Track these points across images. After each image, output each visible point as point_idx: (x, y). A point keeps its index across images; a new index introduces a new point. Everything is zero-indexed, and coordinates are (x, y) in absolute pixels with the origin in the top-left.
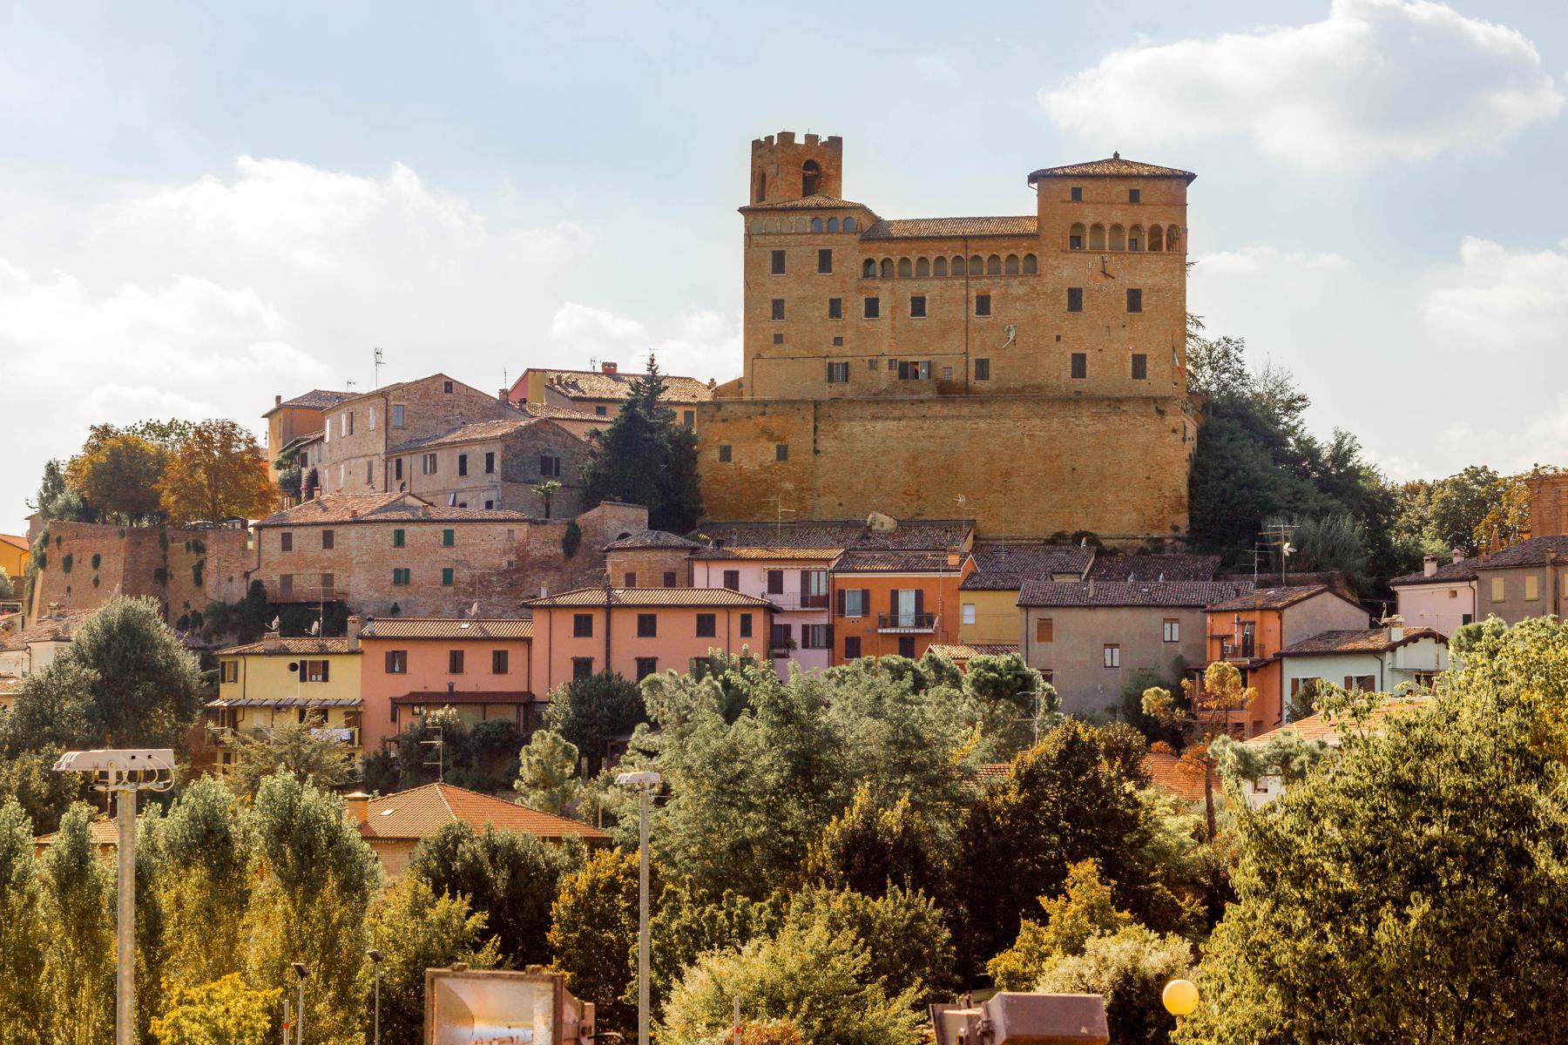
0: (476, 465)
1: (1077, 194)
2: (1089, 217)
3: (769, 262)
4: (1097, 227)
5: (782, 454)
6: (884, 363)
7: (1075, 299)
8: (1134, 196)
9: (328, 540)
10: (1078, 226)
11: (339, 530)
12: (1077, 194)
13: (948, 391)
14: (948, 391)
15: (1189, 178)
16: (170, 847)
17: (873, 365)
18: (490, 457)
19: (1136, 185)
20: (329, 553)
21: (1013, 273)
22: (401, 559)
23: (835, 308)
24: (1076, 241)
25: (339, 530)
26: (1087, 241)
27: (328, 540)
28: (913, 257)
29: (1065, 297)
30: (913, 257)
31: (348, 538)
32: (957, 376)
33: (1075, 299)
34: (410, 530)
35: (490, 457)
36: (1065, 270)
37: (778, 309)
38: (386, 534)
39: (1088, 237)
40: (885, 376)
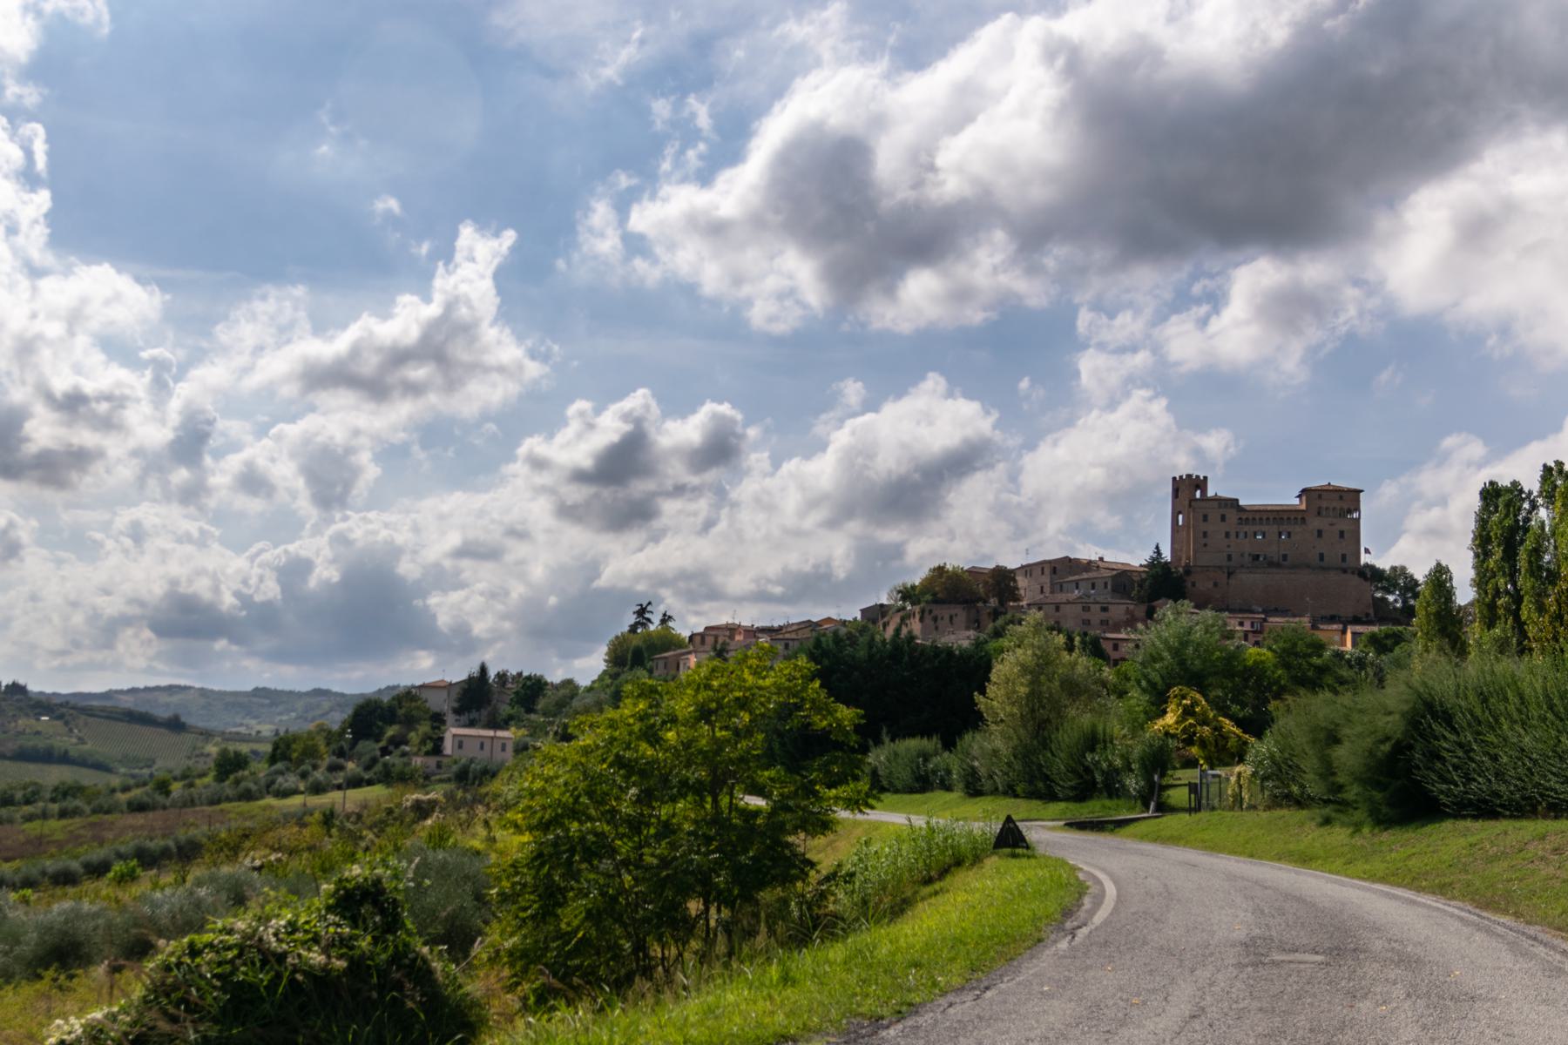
0: (1100, 584)
1: (1320, 496)
2: (1324, 504)
3: (1201, 518)
4: (1327, 508)
5: (1216, 585)
6: (1246, 555)
7: (1320, 533)
8: (1341, 498)
9: (1057, 609)
10: (1320, 508)
11: (1062, 606)
12: (1320, 496)
13: (1272, 564)
14: (1272, 564)
15: (1362, 491)
16: (1142, 760)
17: (1242, 555)
18: (1106, 584)
19: (1343, 494)
20: (1057, 614)
21: (1296, 523)
22: (1086, 616)
23: (1227, 535)
24: (1319, 514)
25: (1062, 606)
26: (1324, 513)
27: (1057, 609)
28: (1264, 517)
29: (1316, 533)
30: (1264, 517)
31: (1066, 609)
32: (1275, 560)
33: (1320, 533)
34: (791, 643)
35: (1106, 584)
36: (1315, 523)
37: (1205, 534)
38: (1079, 607)
39: (629, 658)
40: (1247, 559)
